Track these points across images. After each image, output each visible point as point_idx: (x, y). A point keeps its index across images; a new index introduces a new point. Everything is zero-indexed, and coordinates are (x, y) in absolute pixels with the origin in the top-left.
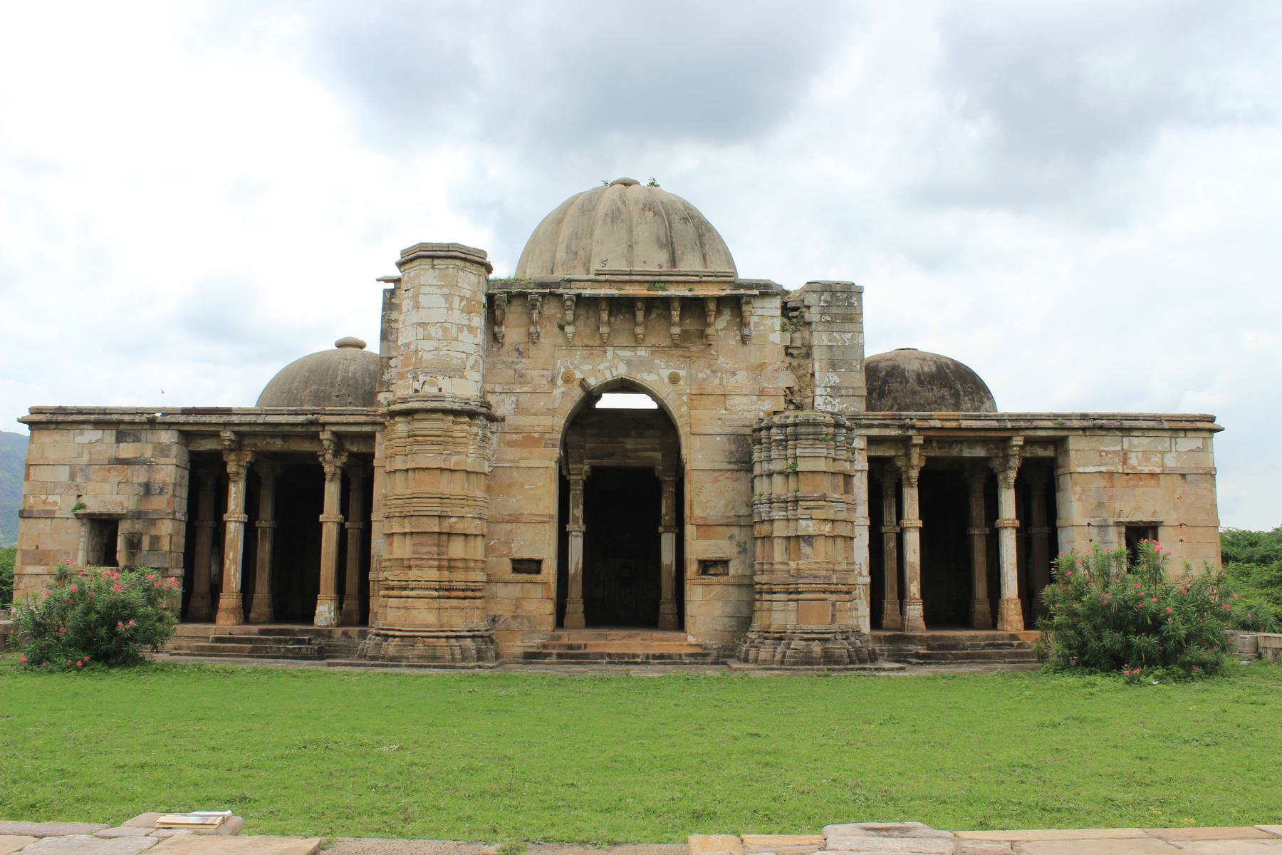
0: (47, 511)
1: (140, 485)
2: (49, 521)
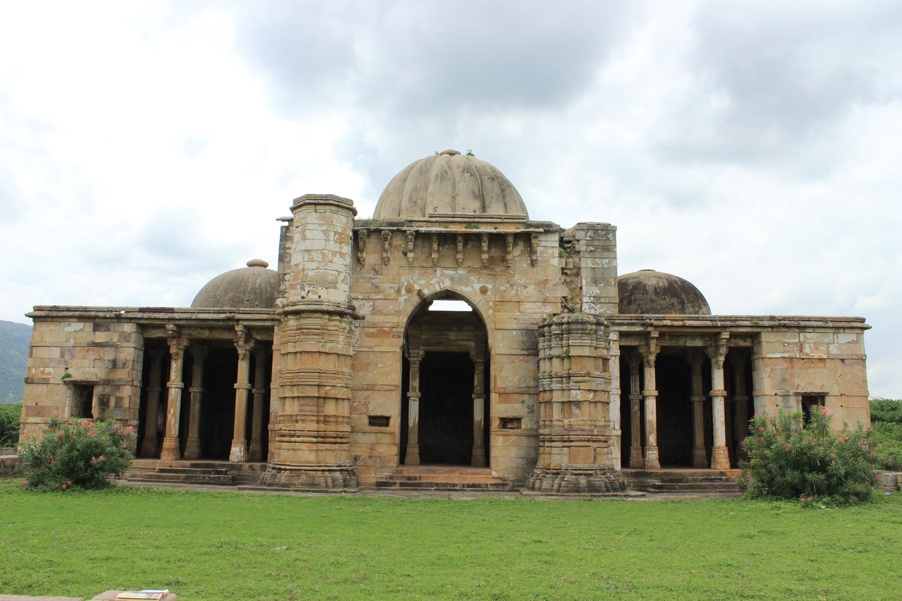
0: (45, 379)
1: (109, 361)
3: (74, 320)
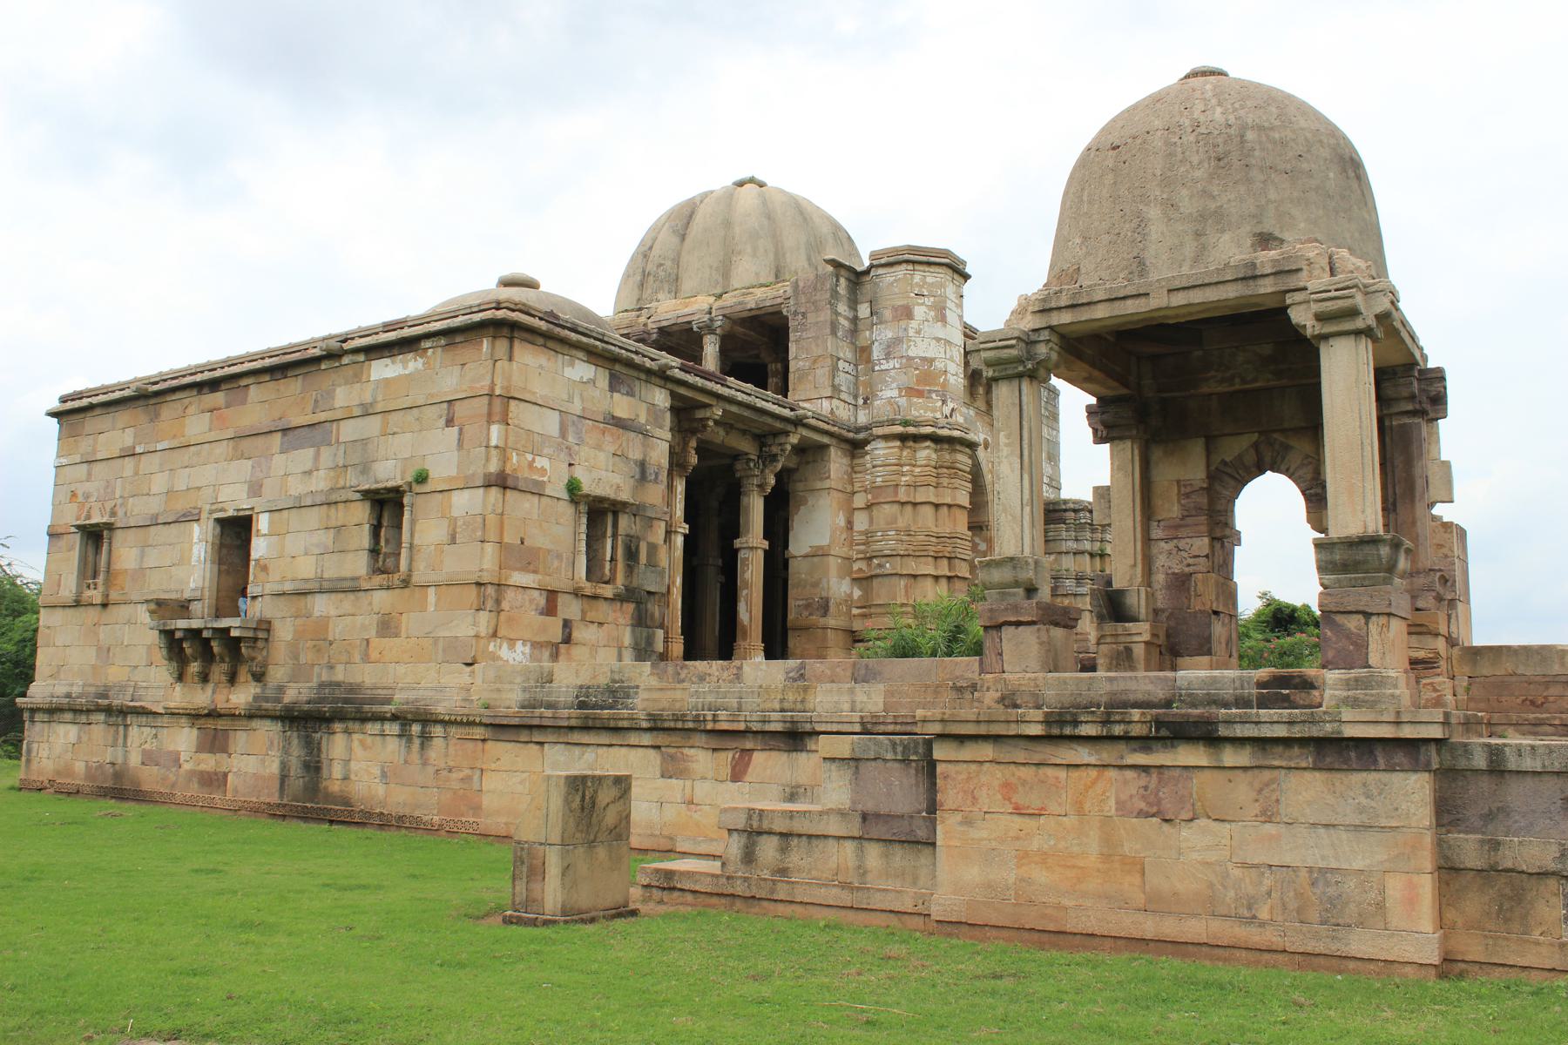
0: (536, 483)
1: (636, 462)
2: (536, 498)
3: (581, 355)
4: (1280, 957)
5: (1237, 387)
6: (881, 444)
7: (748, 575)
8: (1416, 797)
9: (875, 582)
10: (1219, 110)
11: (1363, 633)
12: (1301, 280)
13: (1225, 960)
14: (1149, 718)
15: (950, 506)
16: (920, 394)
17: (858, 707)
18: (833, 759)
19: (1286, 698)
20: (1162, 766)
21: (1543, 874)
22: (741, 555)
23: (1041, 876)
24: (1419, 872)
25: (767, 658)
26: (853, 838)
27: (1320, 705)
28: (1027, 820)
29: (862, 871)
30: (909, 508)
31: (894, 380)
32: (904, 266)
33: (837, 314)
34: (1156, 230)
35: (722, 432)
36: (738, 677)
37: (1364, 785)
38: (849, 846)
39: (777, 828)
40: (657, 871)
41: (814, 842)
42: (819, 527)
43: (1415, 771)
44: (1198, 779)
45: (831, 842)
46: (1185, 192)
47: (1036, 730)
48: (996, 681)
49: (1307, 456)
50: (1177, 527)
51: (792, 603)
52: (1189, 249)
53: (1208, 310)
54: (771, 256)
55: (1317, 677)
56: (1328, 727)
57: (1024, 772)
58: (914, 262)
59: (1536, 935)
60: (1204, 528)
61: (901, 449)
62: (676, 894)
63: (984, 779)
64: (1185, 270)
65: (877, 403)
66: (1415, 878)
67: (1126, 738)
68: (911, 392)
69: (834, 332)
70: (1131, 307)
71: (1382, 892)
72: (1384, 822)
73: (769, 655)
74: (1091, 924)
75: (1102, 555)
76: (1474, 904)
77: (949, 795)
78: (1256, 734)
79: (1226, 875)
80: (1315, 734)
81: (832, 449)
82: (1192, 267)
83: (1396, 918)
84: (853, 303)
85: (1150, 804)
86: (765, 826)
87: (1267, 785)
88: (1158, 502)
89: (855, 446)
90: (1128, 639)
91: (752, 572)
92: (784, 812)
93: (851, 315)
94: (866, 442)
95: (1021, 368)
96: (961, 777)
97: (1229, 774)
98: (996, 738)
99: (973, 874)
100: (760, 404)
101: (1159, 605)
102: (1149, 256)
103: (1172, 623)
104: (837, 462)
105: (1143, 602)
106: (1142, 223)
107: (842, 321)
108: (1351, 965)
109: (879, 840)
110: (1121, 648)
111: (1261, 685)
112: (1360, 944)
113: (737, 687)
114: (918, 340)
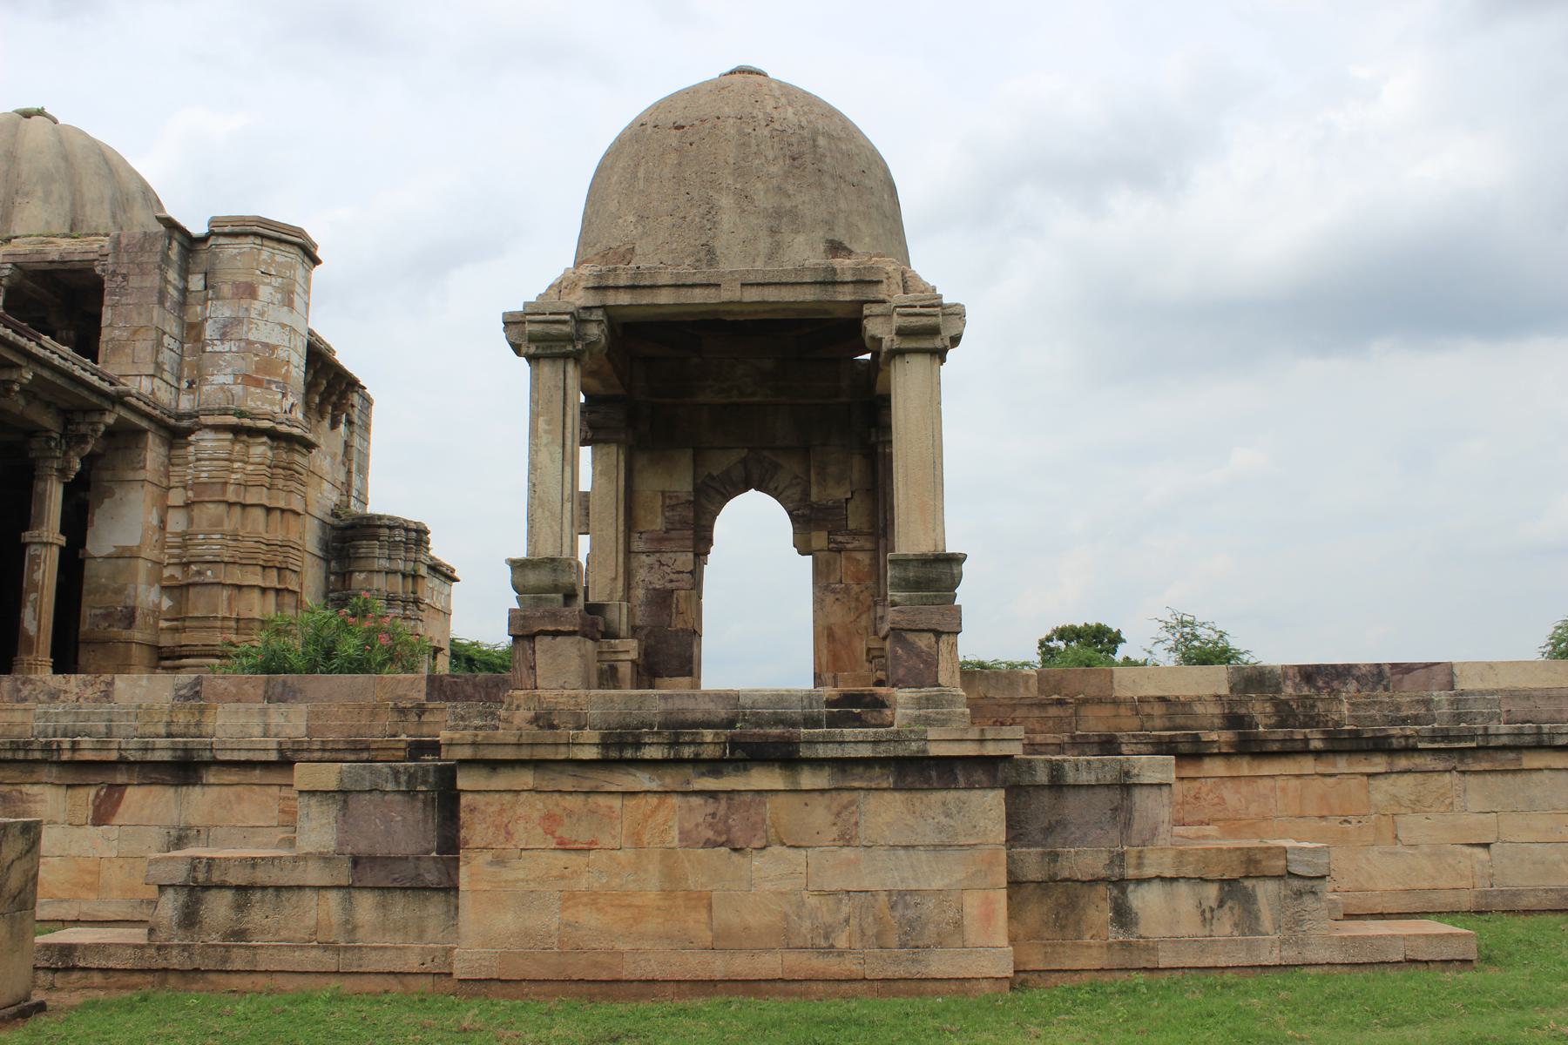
4: (858, 986)
5: (735, 399)
6: (209, 435)
7: (38, 576)
8: (993, 814)
9: (192, 591)
10: (790, 110)
11: (933, 651)
12: (881, 292)
13: (801, 995)
14: (723, 739)
15: (283, 511)
16: (258, 383)
17: (273, 731)
18: (312, 793)
19: (857, 717)
20: (733, 791)
21: (1094, 882)
22: (31, 551)
23: (589, 918)
24: (995, 887)
25: (56, 672)
26: (339, 887)
27: (892, 724)
28: (573, 855)
29: (350, 927)
30: (238, 509)
31: (229, 364)
32: (251, 239)
33: (167, 281)
34: (727, 220)
35: (22, 402)
36: (107, 695)
37: (944, 804)
38: (333, 898)
39: (232, 879)
40: (47, 947)
41: (285, 895)
42: (130, 524)
43: (993, 788)
44: (771, 804)
45: (308, 893)
46: (759, 185)
47: (591, 753)
48: (528, 698)
49: (796, 477)
50: (661, 540)
51: (86, 612)
52: (764, 244)
53: (774, 311)
54: (67, 205)
55: (888, 696)
56: (914, 746)
57: (570, 802)
58: (263, 236)
59: (1087, 939)
60: (689, 543)
61: (233, 442)
62: (75, 976)
63: (520, 811)
64: (759, 265)
65: (205, 388)
66: (991, 893)
67: (696, 761)
68: (248, 380)
69: (161, 302)
70: (699, 296)
71: (960, 910)
72: (962, 841)
73: (58, 669)
74: (652, 968)
75: (415, 576)
76: (1035, 914)
77: (475, 830)
78: (839, 755)
79: (802, 904)
80: (901, 753)
81: (150, 436)
82: (766, 264)
83: (973, 933)
84: (185, 273)
85: (718, 833)
86: (216, 877)
87: (846, 808)
88: (640, 513)
89: (176, 433)
90: (614, 657)
91: (44, 572)
92: (243, 860)
93: (181, 286)
94: (190, 431)
95: (570, 348)
96: (491, 809)
97: (806, 797)
98: (537, 764)
99: (507, 921)
100: (78, 372)
101: (638, 622)
102: (719, 245)
103: (652, 642)
104: (153, 452)
105: (624, 619)
106: (711, 211)
107: (171, 290)
108: (930, 986)
109: (373, 888)
110: (605, 666)
111: (830, 703)
112: (939, 964)
113: (105, 708)
114: (261, 324)
